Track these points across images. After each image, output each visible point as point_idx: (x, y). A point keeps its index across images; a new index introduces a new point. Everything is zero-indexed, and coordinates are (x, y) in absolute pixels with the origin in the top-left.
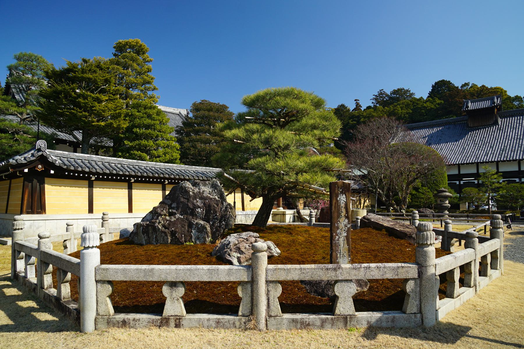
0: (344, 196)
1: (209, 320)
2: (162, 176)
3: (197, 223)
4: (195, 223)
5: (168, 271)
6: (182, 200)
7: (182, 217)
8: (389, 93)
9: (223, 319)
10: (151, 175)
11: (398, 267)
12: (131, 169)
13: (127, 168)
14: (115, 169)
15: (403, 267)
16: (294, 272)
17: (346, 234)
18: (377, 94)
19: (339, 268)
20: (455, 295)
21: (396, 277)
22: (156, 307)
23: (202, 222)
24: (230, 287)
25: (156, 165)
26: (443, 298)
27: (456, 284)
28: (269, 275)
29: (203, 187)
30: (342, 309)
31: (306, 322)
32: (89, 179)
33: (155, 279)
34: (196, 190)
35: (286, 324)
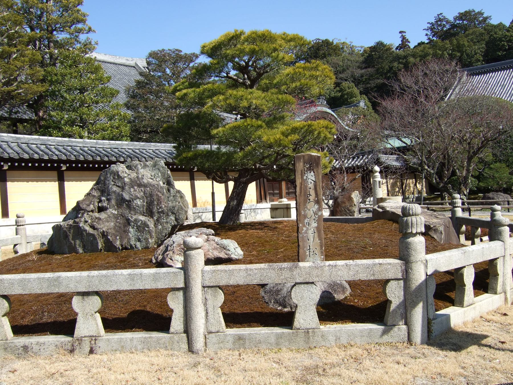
0: (312, 173)
1: (132, 340)
2: (106, 159)
3: (136, 220)
4: (132, 220)
5: (78, 279)
6: (115, 188)
7: (116, 213)
8: (451, 19)
9: (150, 337)
10: (90, 158)
11: (375, 265)
12: (60, 151)
13: (54, 150)
14: (37, 153)
15: (380, 264)
16: (241, 274)
17: (316, 225)
18: (433, 21)
19: (296, 267)
20: (465, 303)
21: (372, 278)
22: (66, 327)
23: (142, 218)
24: (160, 295)
25: (97, 143)
26: (448, 307)
27: (466, 288)
28: (207, 279)
29: (142, 170)
30: (302, 321)
31: (256, 338)
32: (58, 169)
33: (62, 290)
34: (134, 175)
35: (230, 342)
